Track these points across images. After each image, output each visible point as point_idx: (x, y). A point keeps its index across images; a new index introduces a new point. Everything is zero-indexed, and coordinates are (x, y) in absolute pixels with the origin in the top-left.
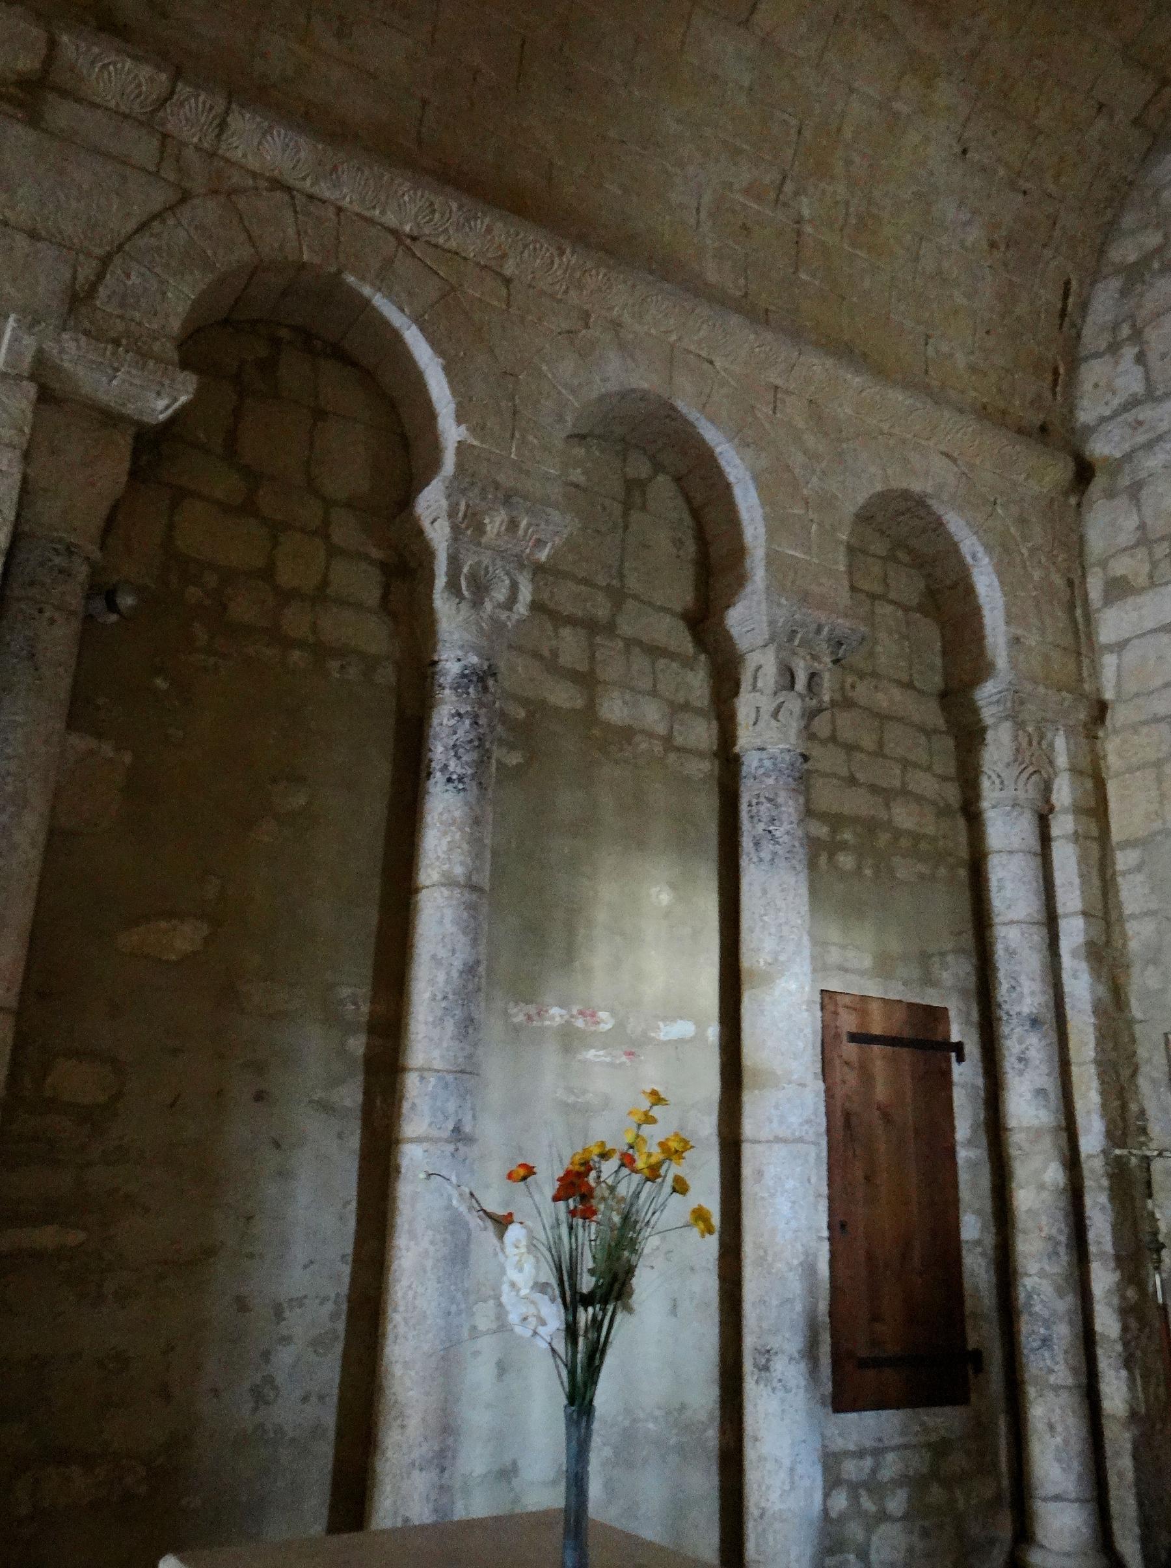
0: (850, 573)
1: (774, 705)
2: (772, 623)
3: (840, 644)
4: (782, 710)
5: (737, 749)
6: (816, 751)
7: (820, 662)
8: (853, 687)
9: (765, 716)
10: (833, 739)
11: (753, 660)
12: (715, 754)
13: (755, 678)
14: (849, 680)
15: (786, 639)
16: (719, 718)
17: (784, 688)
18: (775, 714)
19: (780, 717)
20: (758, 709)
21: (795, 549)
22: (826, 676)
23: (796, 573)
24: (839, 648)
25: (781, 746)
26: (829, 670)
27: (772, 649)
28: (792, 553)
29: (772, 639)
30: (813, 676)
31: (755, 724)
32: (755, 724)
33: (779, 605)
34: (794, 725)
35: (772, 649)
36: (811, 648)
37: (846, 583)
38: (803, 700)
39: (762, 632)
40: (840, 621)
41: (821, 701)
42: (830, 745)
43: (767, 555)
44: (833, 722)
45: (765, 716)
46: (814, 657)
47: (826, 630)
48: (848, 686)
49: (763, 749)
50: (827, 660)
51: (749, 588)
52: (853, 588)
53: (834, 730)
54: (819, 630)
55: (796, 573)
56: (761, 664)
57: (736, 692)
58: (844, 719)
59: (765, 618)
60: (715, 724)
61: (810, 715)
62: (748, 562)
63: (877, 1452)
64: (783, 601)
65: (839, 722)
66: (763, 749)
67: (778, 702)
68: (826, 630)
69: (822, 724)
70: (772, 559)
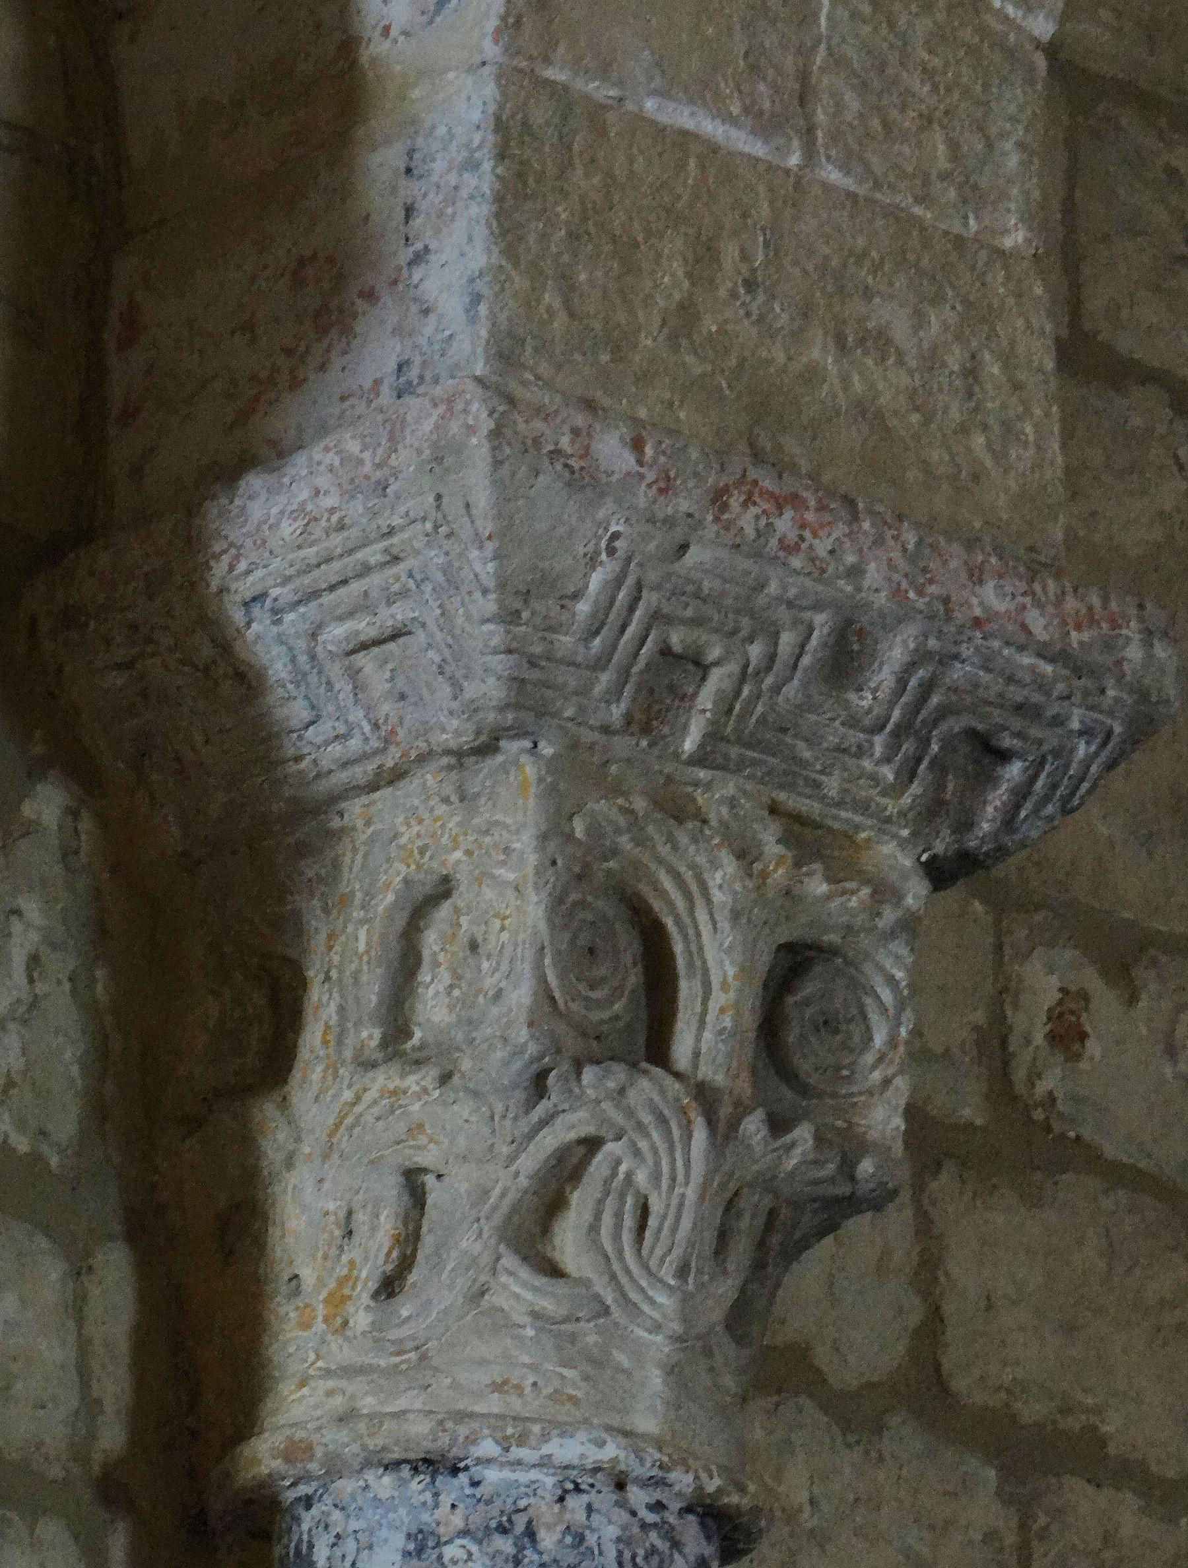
0: (1069, 251)
1: (531, 1161)
2: (528, 595)
3: (988, 751)
4: (580, 1200)
5: (263, 1455)
6: (807, 1472)
7: (842, 871)
8: (1067, 1035)
9: (463, 1236)
10: (922, 1385)
11: (391, 839)
12: (112, 1490)
13: (406, 966)
14: (1043, 981)
15: (616, 709)
16: (148, 1229)
17: (597, 1048)
18: (531, 1232)
19: (568, 1242)
20: (414, 1184)
21: (703, 92)
22: (889, 968)
23: (704, 255)
24: (984, 779)
25: (570, 1450)
26: (909, 926)
27: (521, 773)
28: (684, 117)
29: (531, 701)
30: (793, 968)
31: (389, 1287)
32: (389, 1287)
33: (583, 479)
34: (657, 1314)
35: (521, 773)
36: (793, 775)
37: (1034, 339)
38: (724, 1134)
39: (460, 662)
40: (991, 597)
41: (846, 1146)
42: (904, 1438)
43: (510, 134)
44: (928, 1271)
45: (463, 1236)
46: (808, 839)
47: (895, 651)
48: (1031, 1024)
49: (435, 1465)
50: (895, 856)
51: (377, 353)
52: (1084, 358)
53: (931, 1330)
54: (845, 659)
55: (704, 255)
56: (446, 878)
57: (275, 1064)
58: (1000, 1251)
59: (481, 565)
60: (115, 1269)
61: (766, 1235)
62: (381, 162)
63: (511, 668)
64: (612, 451)
65: (964, 1273)
66: (435, 1465)
67: (550, 1140)
68: (895, 651)
69: (849, 1306)
70: (535, 154)
